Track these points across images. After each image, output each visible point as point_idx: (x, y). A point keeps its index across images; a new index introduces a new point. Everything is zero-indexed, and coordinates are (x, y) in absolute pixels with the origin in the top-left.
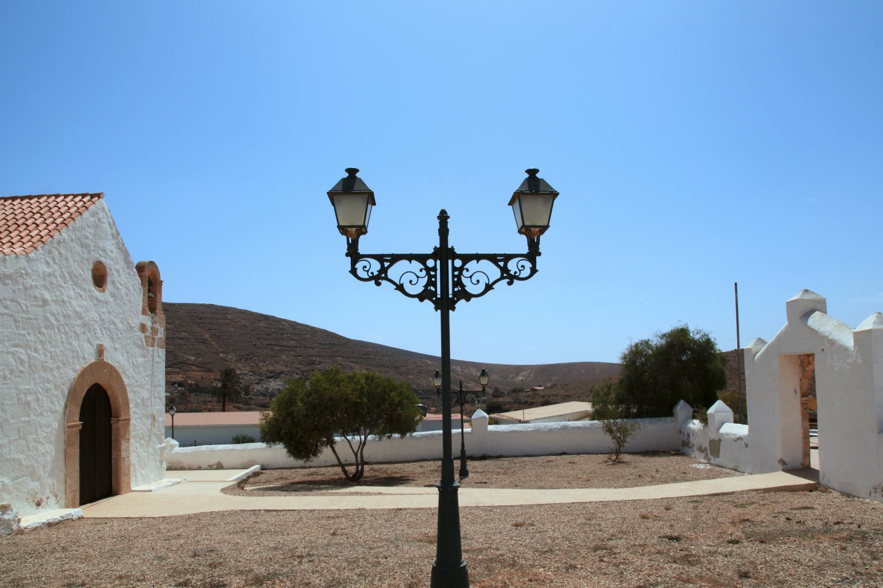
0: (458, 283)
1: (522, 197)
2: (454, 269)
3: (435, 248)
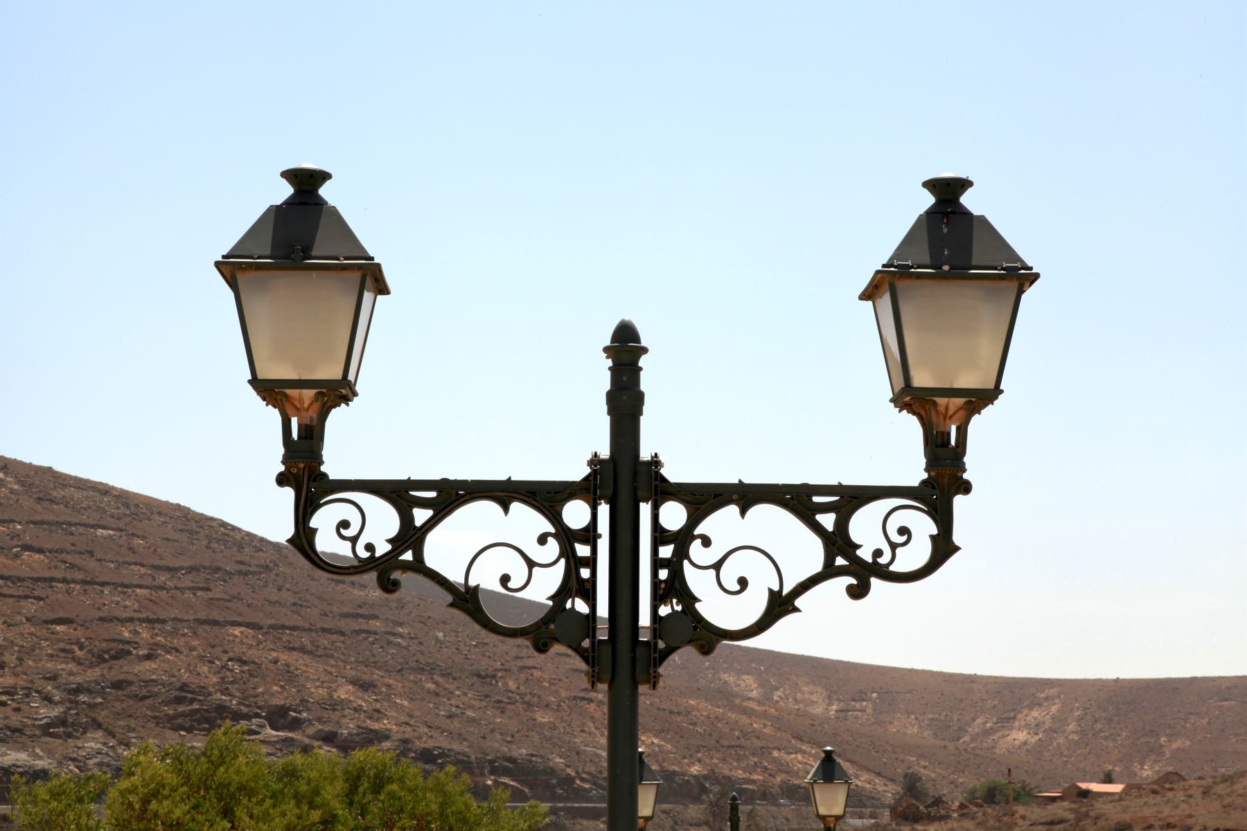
0: (673, 587)
1: (901, 285)
2: (661, 537)
3: (595, 461)
